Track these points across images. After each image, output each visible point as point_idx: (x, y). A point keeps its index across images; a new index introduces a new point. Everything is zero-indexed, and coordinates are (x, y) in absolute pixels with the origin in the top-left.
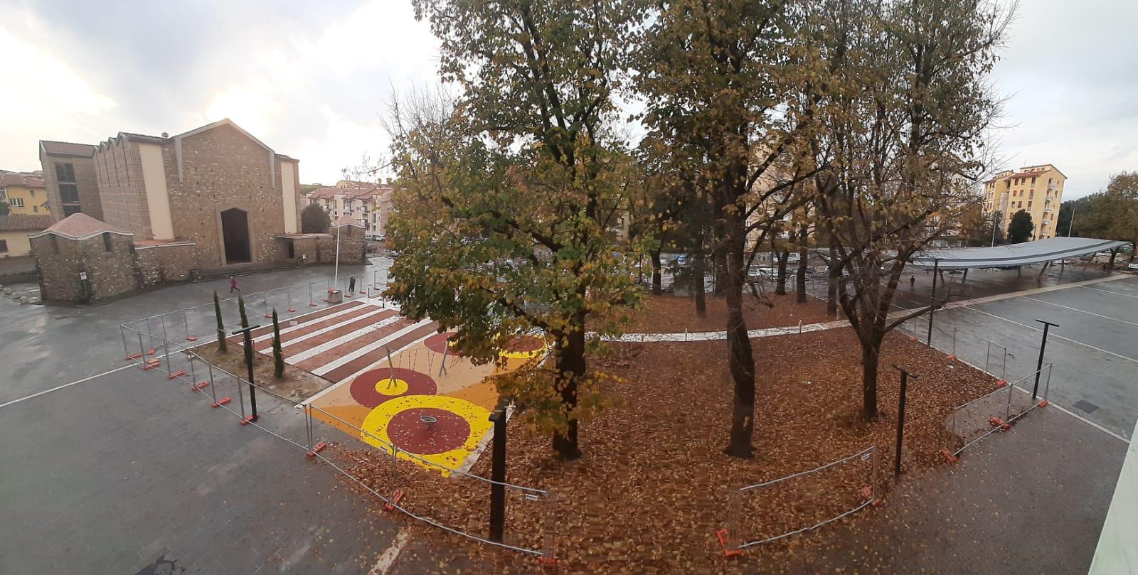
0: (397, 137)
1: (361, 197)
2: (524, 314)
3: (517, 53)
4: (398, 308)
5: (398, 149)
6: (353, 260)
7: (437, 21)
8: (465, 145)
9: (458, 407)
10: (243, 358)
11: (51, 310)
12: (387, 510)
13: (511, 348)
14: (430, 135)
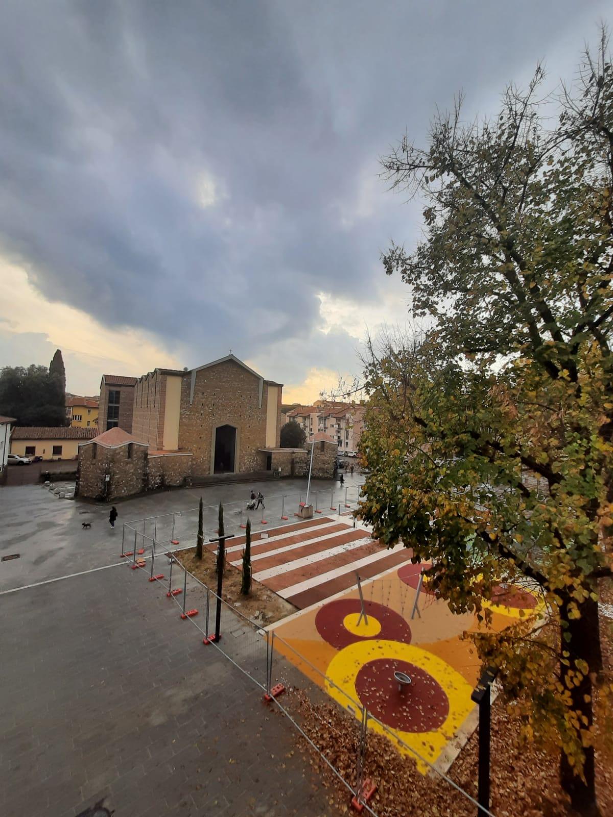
0: (370, 365)
1: (335, 415)
2: (514, 557)
3: (497, 282)
4: (370, 529)
5: (370, 374)
6: (330, 476)
7: (408, 272)
8: (438, 368)
9: (436, 669)
10: (215, 568)
11: (79, 505)
12: (353, 808)
13: (496, 599)
14: (401, 361)
